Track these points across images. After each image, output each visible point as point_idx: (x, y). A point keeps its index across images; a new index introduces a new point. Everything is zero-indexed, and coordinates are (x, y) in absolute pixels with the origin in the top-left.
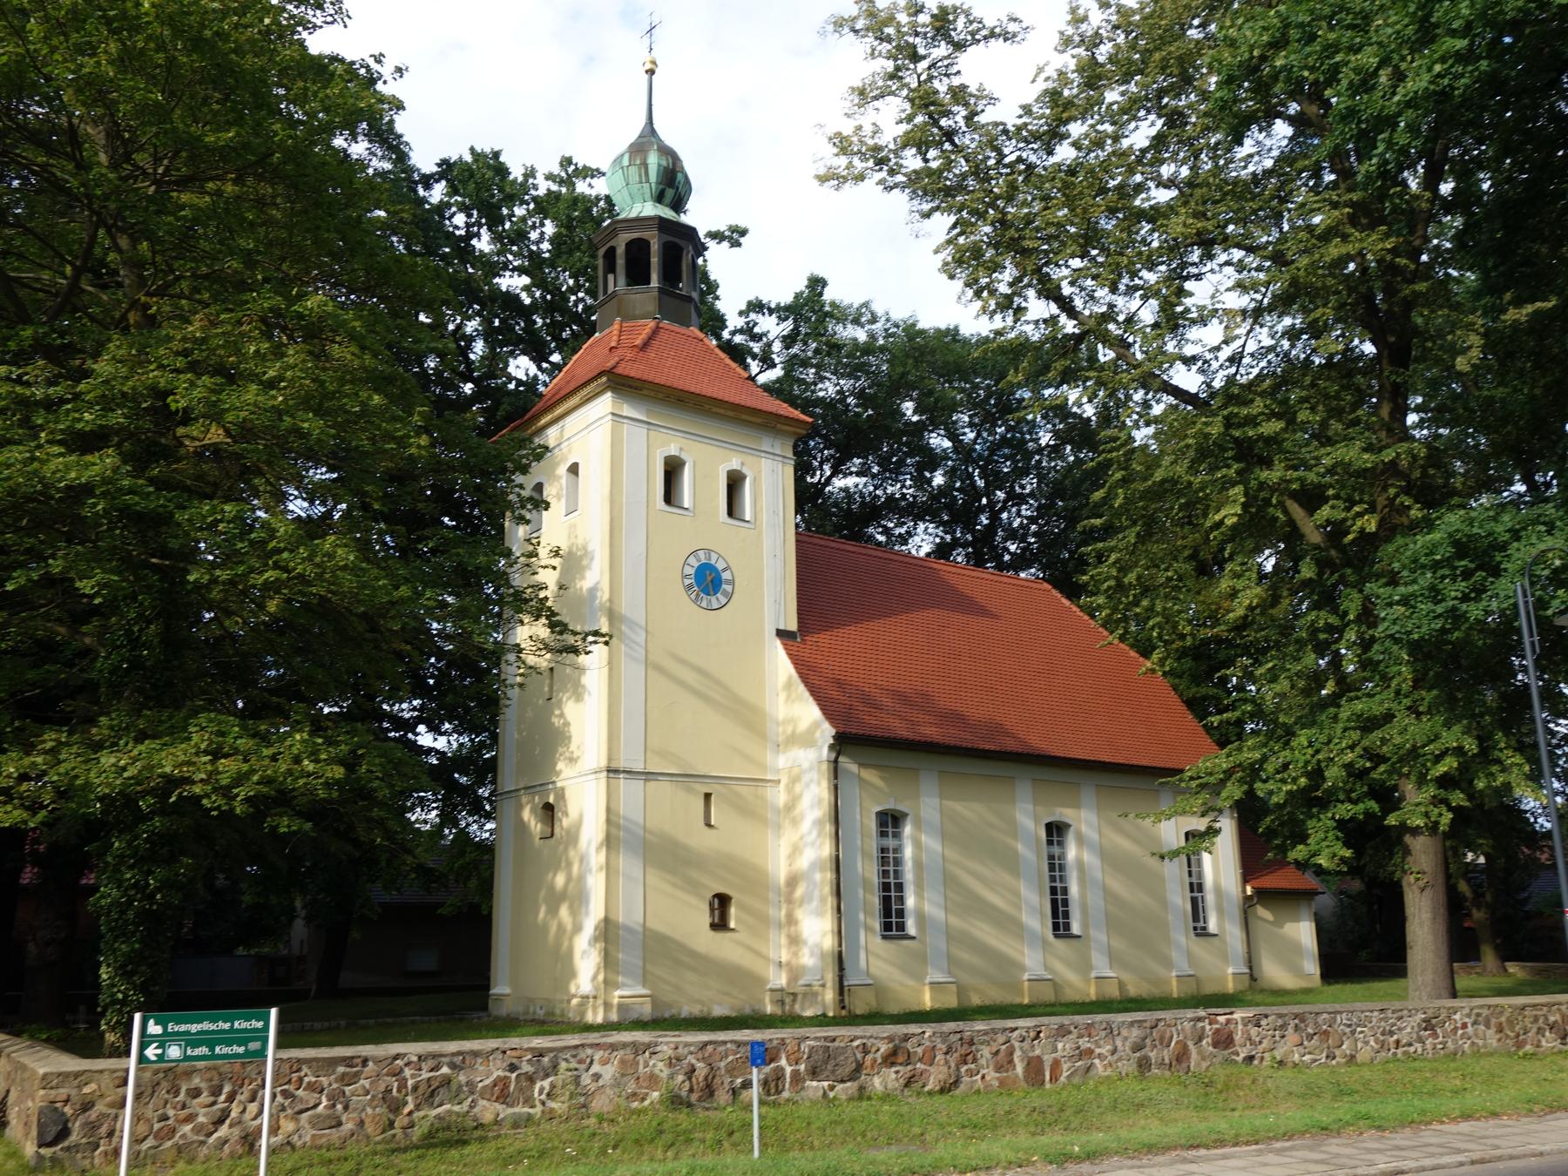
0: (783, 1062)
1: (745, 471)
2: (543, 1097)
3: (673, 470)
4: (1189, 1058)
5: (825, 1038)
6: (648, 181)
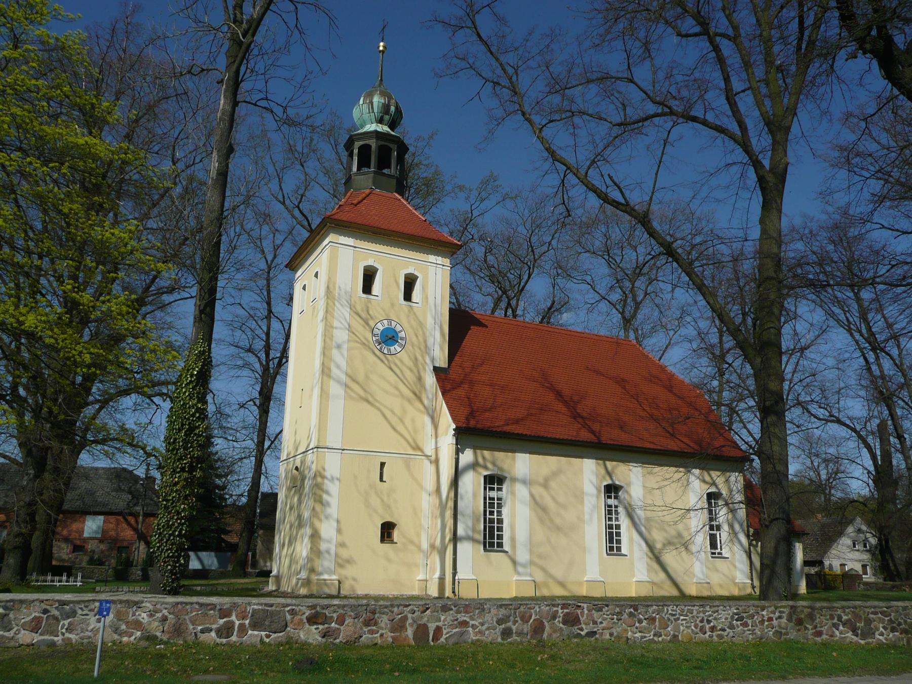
0: (233, 618)
1: (376, 265)
2: (64, 631)
3: (369, 277)
4: (543, 631)
5: (266, 605)
6: (373, 112)
